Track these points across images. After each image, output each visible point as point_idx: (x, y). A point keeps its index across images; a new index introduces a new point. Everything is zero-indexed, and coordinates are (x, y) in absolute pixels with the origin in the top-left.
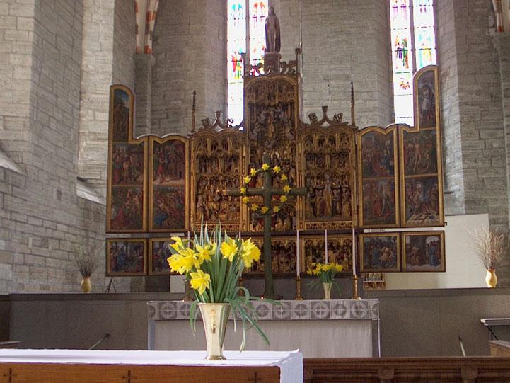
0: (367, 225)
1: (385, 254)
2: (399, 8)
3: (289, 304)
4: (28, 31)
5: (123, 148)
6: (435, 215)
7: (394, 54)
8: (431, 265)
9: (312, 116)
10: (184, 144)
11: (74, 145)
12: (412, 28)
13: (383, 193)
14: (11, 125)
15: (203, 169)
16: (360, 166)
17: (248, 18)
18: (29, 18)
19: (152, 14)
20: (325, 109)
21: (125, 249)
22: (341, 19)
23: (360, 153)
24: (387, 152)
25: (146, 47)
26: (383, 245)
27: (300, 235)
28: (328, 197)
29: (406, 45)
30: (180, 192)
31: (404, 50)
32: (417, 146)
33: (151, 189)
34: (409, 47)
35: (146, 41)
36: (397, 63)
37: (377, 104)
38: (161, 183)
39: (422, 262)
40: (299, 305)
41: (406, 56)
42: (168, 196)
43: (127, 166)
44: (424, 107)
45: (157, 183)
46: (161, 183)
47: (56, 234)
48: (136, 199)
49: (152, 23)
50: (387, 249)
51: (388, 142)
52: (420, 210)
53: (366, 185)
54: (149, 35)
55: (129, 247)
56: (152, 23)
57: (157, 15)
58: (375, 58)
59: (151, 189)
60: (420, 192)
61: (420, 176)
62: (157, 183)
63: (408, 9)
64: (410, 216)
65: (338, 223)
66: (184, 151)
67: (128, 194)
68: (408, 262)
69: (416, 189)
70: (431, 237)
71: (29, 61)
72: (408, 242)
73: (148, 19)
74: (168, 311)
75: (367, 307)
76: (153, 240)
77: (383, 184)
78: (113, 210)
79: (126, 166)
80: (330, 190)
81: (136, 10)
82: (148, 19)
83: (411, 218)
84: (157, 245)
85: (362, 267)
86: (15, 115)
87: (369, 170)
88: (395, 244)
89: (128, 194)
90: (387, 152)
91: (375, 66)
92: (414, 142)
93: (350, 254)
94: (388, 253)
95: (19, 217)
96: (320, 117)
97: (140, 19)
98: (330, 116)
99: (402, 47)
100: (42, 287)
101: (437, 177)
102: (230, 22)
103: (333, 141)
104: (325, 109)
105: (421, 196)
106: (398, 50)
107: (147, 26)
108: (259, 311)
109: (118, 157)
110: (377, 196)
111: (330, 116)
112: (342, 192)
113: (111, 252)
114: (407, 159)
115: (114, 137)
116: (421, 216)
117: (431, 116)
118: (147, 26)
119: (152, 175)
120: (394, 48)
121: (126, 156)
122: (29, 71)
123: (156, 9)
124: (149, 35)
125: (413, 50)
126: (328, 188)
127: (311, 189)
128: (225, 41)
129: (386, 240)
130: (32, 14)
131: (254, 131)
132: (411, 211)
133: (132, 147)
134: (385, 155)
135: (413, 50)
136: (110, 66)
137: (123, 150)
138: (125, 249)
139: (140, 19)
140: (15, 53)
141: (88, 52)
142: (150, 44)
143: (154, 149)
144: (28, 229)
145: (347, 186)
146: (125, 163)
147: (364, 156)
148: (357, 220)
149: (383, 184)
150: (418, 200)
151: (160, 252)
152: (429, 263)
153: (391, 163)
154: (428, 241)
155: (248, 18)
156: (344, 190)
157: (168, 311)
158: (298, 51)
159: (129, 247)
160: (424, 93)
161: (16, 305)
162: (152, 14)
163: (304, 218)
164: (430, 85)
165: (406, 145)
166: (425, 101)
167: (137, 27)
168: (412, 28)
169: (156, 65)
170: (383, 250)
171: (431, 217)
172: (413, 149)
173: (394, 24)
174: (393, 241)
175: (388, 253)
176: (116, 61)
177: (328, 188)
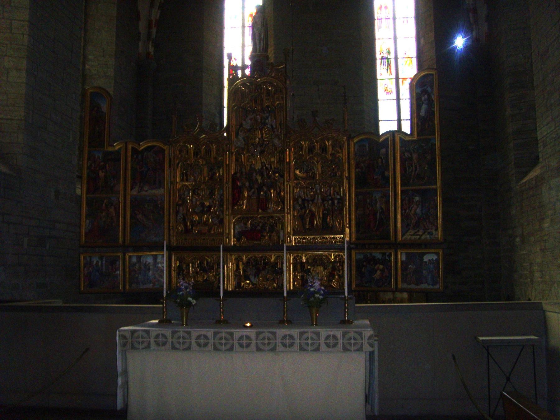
1: (379, 272)
2: (384, 20)
3: (274, 334)
4: (23, 34)
5: (99, 155)
6: (434, 232)
7: (378, 62)
8: (429, 284)
10: (164, 150)
12: (395, 38)
13: (378, 205)
15: (185, 178)
16: (353, 176)
18: (23, 21)
19: (154, 22)
21: (100, 264)
22: (265, 217)
23: (353, 162)
24: (382, 161)
25: (149, 53)
27: (287, 250)
29: (389, 53)
30: (159, 202)
31: (387, 58)
32: (415, 156)
33: (129, 198)
34: (392, 56)
38: (139, 192)
40: (286, 336)
41: (389, 64)
42: (146, 206)
43: (103, 174)
44: (423, 113)
45: (135, 192)
46: (139, 192)
48: (112, 210)
49: (154, 30)
50: (381, 267)
51: (383, 151)
53: (360, 197)
54: (151, 43)
55: (104, 262)
56: (154, 30)
59: (129, 198)
60: (418, 206)
61: (417, 187)
62: (135, 192)
63: (391, 21)
64: (406, 232)
66: (164, 158)
67: (104, 205)
68: (404, 280)
69: (413, 202)
70: (430, 255)
71: (24, 64)
72: (404, 258)
74: (141, 340)
75: (362, 339)
76: (131, 254)
77: (377, 195)
78: (88, 221)
79: (101, 174)
80: (320, 201)
81: (138, 18)
83: (408, 234)
84: (134, 260)
85: (354, 286)
86: (9, 117)
87: (362, 181)
88: (390, 261)
89: (104, 205)
90: (382, 161)
92: (412, 151)
93: (341, 272)
94: (382, 271)
97: (142, 26)
99: (385, 55)
101: (436, 190)
105: (418, 211)
106: (382, 58)
107: (149, 34)
108: (241, 342)
109: (93, 165)
110: (371, 208)
112: (333, 203)
113: (84, 268)
114: (403, 170)
115: (90, 143)
116: (418, 231)
117: (431, 123)
118: (149, 34)
119: (129, 185)
120: (378, 56)
121: (102, 163)
122: (24, 74)
123: (158, 18)
124: (151, 43)
125: (396, 58)
127: (300, 200)
129: (380, 257)
130: (27, 18)
131: (240, 138)
132: (407, 226)
134: (380, 164)
135: (396, 58)
136: (112, 70)
137: (99, 157)
138: (100, 264)
140: (9, 56)
141: (90, 57)
142: (151, 49)
143: (132, 156)
145: (338, 197)
146: (100, 172)
147: (357, 165)
150: (415, 214)
151: (137, 267)
152: (426, 282)
153: (386, 173)
156: (336, 202)
157: (141, 340)
159: (104, 262)
160: (423, 98)
162: (154, 22)
163: (292, 232)
164: (429, 89)
165: (402, 154)
166: (424, 107)
167: (139, 33)
168: (395, 38)
170: (376, 267)
171: (429, 233)
172: (411, 159)
174: (387, 258)
175: (382, 271)
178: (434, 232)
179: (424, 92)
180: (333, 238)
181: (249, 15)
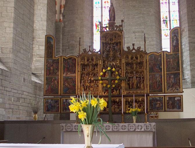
0: (151, 92)
1: (158, 105)
2: (164, 3)
3: (119, 125)
4: (12, 13)
5: (51, 61)
6: (179, 88)
7: (162, 22)
8: (177, 109)
9: (128, 48)
10: (76, 59)
11: (30, 59)
12: (169, 12)
14: (4, 51)
15: (84, 70)
16: (148, 68)
17: (102, 7)
18: (12, 7)
19: (62, 6)
20: (133, 45)
21: (51, 102)
23: (148, 63)
24: (159, 63)
25: (60, 19)
26: (157, 101)
27: (123, 96)
28: (135, 81)
29: (167, 18)
30: (74, 79)
31: (166, 21)
32: (171, 60)
33: (62, 78)
34: (168, 19)
35: (60, 17)
36: (163, 26)
37: (155, 43)
38: (66, 75)
39: (173, 108)
40: (123, 125)
41: (167, 23)
42: (69, 80)
43: (52, 68)
44: (174, 44)
45: (64, 75)
46: (66, 75)
47: (23, 96)
48: (56, 82)
49: (63, 9)
50: (159, 102)
51: (159, 58)
52: (173, 86)
53: (151, 76)
54: (61, 15)
55: (53, 102)
56: (63, 9)
57: (65, 6)
58: (154, 24)
59: (62, 78)
60: (173, 79)
61: (173, 72)
62: (64, 75)
63: (168, 4)
64: (169, 89)
65: (139, 91)
66: (76, 62)
67: (53, 80)
68: (168, 108)
69: (171, 78)
70: (177, 97)
71: (12, 25)
72: (168, 99)
73: (61, 8)
74: (69, 128)
75: (151, 126)
76: (63, 99)
77: (157, 76)
78: (46, 86)
79: (52, 68)
80: (135, 78)
81: (56, 4)
82: (61, 8)
83: (169, 90)
84: (65, 101)
85: (149, 110)
86: (6, 47)
87: (152, 70)
88: (162, 100)
89: (53, 80)
90: (159, 63)
91: (154, 27)
92: (170, 58)
93: (144, 104)
94: (160, 104)
95: (8, 89)
96: (131, 48)
97: (57, 8)
98: (136, 48)
99: (165, 19)
100: (17, 118)
101: (179, 73)
102: (94, 9)
103: (137, 58)
104: (133, 45)
105: (173, 81)
106: (164, 21)
107: (61, 11)
108: (107, 128)
109: (48, 65)
110: (155, 80)
111: (136, 48)
113: (45, 104)
114: (167, 65)
115: (47, 56)
116: (173, 89)
117: (177, 48)
118: (61, 11)
119: (62, 72)
120: (162, 20)
121: (52, 64)
122: (12, 29)
123: (64, 4)
124: (61, 15)
125: (170, 21)
126: (135, 77)
127: (128, 78)
128: (92, 17)
129: (159, 99)
130: (13, 6)
131: (105, 54)
132: (169, 87)
133: (54, 60)
134: (158, 64)
135: (170, 21)
136: (45, 27)
137: (50, 62)
138: (51, 102)
139: (57, 8)
140: (6, 22)
141: (36, 21)
142: (61, 18)
143: (63, 61)
144: (12, 94)
146: (51, 67)
147: (150, 64)
148: (147, 90)
149: (157, 76)
150: (172, 82)
151: (66, 103)
152: (176, 108)
153: (161, 67)
154: (176, 99)
155: (102, 7)
156: (141, 78)
157: (69, 128)
158: (122, 21)
159: (53, 102)
160: (174, 38)
161: (7, 125)
162: (62, 6)
164: (177, 35)
165: (167, 59)
166: (175, 41)
167: (56, 11)
168: (169, 12)
169: (64, 27)
170: (157, 103)
171: (177, 89)
172: (170, 61)
173: (162, 10)
174: (161, 99)
175: (160, 104)
176: (48, 25)
177: (135, 77)
178: (179, 88)
179: (175, 36)
180: (141, 92)
181: (104, 2)
